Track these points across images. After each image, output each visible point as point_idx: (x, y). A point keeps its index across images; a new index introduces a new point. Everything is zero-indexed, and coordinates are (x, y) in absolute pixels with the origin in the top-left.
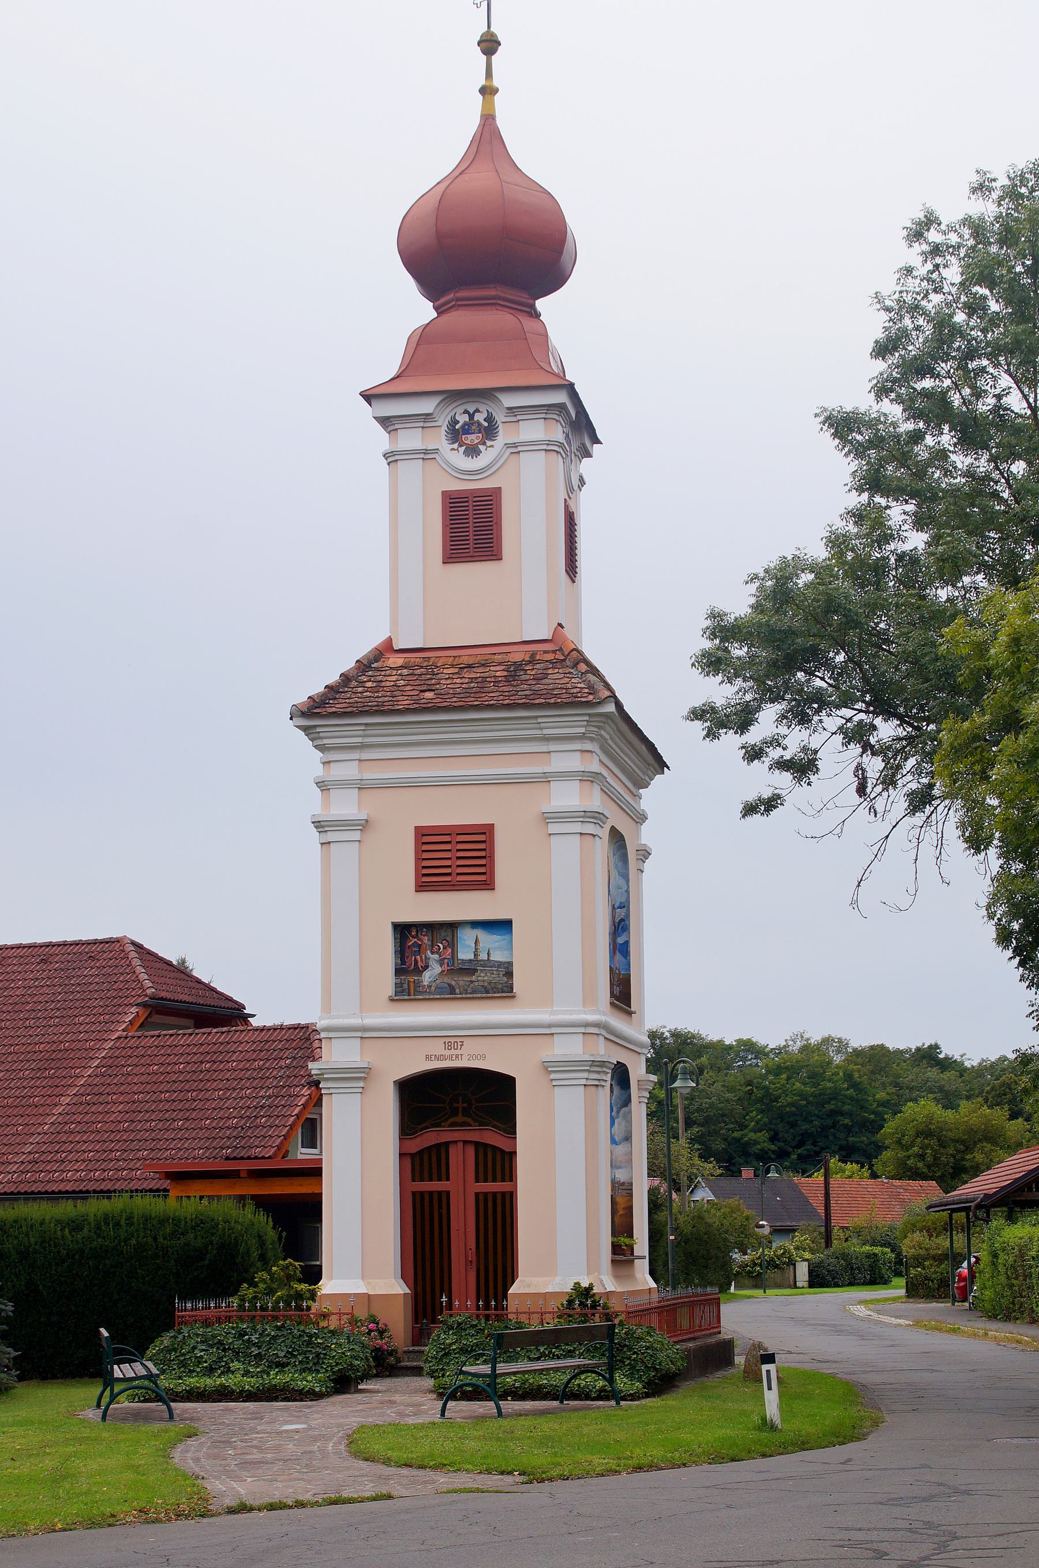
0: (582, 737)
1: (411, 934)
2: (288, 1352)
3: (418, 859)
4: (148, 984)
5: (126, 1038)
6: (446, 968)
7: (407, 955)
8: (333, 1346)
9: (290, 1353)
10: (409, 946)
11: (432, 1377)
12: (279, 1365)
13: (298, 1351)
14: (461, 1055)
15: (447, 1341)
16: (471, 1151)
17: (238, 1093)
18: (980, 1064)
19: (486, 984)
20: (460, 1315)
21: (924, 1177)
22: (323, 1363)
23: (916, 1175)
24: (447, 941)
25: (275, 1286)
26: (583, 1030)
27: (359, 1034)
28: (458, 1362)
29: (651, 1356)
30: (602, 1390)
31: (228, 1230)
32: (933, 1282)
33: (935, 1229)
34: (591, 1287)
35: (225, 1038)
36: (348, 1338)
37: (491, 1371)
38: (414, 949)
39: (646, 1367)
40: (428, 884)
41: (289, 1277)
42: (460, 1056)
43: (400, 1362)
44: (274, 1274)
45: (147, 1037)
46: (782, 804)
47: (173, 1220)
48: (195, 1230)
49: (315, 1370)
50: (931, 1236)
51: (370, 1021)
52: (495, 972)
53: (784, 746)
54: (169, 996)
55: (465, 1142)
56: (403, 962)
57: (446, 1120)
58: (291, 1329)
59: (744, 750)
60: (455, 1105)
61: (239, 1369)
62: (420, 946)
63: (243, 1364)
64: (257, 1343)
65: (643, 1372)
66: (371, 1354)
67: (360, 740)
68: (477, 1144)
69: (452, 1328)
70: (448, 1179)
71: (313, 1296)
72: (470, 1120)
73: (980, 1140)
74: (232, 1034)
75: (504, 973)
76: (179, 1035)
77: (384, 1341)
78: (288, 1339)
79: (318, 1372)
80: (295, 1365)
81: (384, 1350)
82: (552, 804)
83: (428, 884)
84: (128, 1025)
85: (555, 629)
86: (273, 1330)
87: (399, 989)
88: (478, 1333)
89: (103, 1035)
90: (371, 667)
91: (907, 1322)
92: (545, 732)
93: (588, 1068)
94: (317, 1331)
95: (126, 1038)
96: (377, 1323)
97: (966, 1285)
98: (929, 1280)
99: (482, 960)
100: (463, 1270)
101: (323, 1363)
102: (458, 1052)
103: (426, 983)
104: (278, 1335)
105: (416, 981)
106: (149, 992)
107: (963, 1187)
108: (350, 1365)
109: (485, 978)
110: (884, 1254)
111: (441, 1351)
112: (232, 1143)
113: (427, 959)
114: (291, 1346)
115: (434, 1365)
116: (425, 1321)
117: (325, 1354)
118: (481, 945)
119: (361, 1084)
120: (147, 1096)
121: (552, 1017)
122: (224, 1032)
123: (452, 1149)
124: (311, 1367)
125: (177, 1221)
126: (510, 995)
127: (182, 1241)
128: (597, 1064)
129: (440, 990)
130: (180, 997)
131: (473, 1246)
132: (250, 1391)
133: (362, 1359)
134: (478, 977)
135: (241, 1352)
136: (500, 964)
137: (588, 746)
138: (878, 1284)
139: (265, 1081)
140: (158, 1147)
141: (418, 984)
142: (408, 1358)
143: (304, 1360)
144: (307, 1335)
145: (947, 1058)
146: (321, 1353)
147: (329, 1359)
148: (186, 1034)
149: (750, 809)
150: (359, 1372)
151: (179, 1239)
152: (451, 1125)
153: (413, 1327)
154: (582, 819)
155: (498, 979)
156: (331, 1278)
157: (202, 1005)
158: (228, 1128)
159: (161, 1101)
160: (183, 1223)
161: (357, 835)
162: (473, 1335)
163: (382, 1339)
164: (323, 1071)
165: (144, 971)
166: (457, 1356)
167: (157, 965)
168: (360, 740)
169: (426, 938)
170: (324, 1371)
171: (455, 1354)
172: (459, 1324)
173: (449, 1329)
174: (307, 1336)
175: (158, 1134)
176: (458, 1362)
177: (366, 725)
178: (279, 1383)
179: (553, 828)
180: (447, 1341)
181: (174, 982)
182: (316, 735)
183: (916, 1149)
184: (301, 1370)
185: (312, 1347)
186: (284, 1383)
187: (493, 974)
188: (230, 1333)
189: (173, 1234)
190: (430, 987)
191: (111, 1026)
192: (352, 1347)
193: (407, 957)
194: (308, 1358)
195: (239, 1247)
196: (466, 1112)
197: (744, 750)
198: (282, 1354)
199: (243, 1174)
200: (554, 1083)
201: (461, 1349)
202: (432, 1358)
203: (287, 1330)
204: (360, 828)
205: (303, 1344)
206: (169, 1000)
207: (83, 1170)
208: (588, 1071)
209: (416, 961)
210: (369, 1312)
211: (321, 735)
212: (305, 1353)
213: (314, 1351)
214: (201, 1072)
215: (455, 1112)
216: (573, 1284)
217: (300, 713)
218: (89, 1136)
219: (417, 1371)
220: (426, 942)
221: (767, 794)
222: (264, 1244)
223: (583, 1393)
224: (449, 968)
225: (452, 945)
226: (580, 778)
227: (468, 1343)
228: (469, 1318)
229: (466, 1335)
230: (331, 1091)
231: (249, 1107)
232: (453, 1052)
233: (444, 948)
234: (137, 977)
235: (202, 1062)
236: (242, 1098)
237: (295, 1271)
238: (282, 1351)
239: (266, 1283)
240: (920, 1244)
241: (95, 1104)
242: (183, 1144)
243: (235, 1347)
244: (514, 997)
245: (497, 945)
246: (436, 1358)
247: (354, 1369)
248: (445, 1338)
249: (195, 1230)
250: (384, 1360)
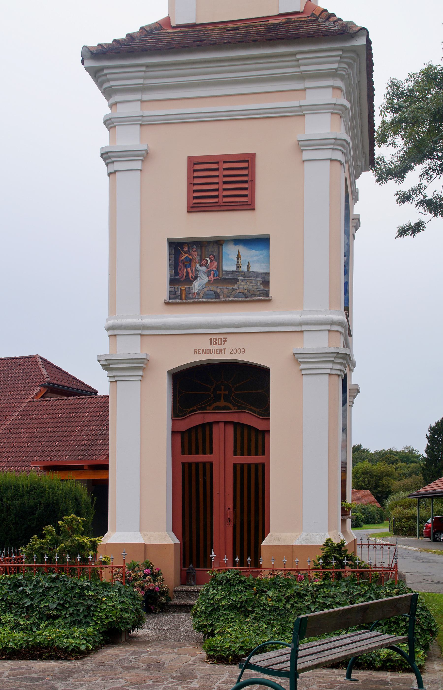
0: (333, 74)
1: (183, 251)
2: (59, 604)
3: (190, 184)
4: (46, 376)
5: (33, 401)
6: (212, 278)
7: (179, 267)
8: (104, 599)
9: (62, 605)
10: (182, 260)
11: (201, 632)
12: (49, 617)
13: (70, 603)
14: (225, 349)
15: (216, 597)
16: (230, 430)
17: (89, 428)
18: (375, 452)
19: (246, 291)
20: (229, 571)
21: (364, 489)
22: (93, 615)
23: (362, 488)
24: (213, 255)
25: (60, 538)
26: (329, 328)
27: (139, 332)
28: (227, 619)
29: (426, 617)
30: (388, 659)
31: (52, 494)
32: (406, 528)
33: (406, 506)
34: (342, 545)
35: (83, 401)
36: (119, 590)
37: (290, 666)
38: (186, 263)
39: (422, 629)
40: (198, 205)
41: (74, 531)
42: (223, 350)
43: (171, 600)
44: (61, 527)
45: (44, 401)
46: (423, 230)
47: (15, 486)
48: (29, 494)
49: (85, 622)
50: (404, 509)
51: (148, 320)
52: (253, 282)
53: (424, 194)
54: (57, 382)
55: (226, 423)
56: (176, 273)
57: (210, 405)
58: (65, 581)
59: (398, 196)
60: (218, 392)
61: (9, 621)
62: (191, 260)
63: (14, 616)
64: (31, 594)
65: (420, 635)
66: (142, 604)
67: (141, 81)
68: (235, 424)
69: (221, 584)
70: (211, 453)
71: (94, 546)
72: (230, 405)
73: (384, 476)
74: (87, 399)
75: (261, 282)
76: (60, 400)
77: (157, 584)
78: (61, 591)
79: (88, 624)
80: (66, 618)
81: (157, 591)
82: (306, 133)
83: (198, 205)
84: (35, 396)
85: (307, 3)
86: (47, 582)
87: (173, 296)
88: (246, 588)
89: (22, 400)
90: (152, 33)
91: (415, 549)
92: (303, 68)
93: (333, 359)
94: (89, 584)
95: (33, 401)
96: (152, 569)
97: (430, 530)
98: (404, 527)
99: (242, 272)
100: (222, 526)
101: (93, 615)
102: (222, 347)
103: (195, 291)
104: (51, 587)
105: (187, 289)
106: (46, 380)
107: (424, 487)
108: (119, 618)
109: (245, 287)
110: (360, 516)
111: (210, 607)
112: (83, 453)
113: (197, 271)
114: (63, 598)
115: (203, 621)
116: (191, 566)
117: (96, 607)
118: (242, 259)
119: (141, 373)
120: (41, 429)
121: (302, 316)
122: (83, 399)
123: (215, 429)
124: (81, 620)
125: (17, 487)
126: (267, 298)
127: (19, 502)
128: (341, 356)
129: (206, 295)
130: (64, 384)
131: (230, 505)
132: (13, 649)
133: (132, 611)
134: (239, 285)
135: (15, 604)
136: (258, 275)
137: (339, 83)
138: (358, 527)
139: (103, 422)
140: (45, 455)
141: (188, 292)
142: (177, 596)
143: (75, 612)
144: (79, 588)
145: (364, 450)
146: (92, 605)
147: (99, 612)
148: (63, 400)
149: (402, 232)
150: (128, 624)
151: (18, 500)
152: (214, 409)
153: (181, 570)
154: (332, 147)
155: (256, 287)
156: (115, 530)
157: (76, 389)
158: (82, 445)
159: (48, 432)
160: (21, 489)
161: (138, 165)
162: (242, 591)
163: (155, 581)
164: (109, 362)
165: (45, 370)
166: (226, 612)
167: (53, 369)
168: (141, 81)
169: (196, 254)
170: (94, 623)
171: (224, 610)
172: (228, 580)
173: (218, 584)
174: (79, 588)
175: (45, 448)
176: (227, 619)
177: (147, 66)
178: (44, 641)
179: (306, 155)
180: (216, 597)
181: (61, 377)
182: (103, 78)
183: (362, 479)
184: (71, 622)
185: (84, 599)
186: (49, 641)
187: (252, 283)
188: (5, 584)
189: (14, 497)
190: (198, 294)
191: (26, 396)
192: (122, 600)
193: (180, 269)
194: (78, 610)
195: (59, 506)
196: (227, 399)
197: (398, 196)
198: (53, 606)
199: (86, 468)
200: (303, 372)
201: (230, 606)
202: (201, 612)
203: (61, 581)
204: (141, 158)
205: (75, 597)
206: (58, 385)
207: (4, 467)
208: (333, 362)
209: (187, 273)
210: (145, 558)
211: (109, 76)
212: (76, 605)
213: (85, 603)
214: (70, 417)
215: (218, 399)
216: (325, 541)
217: (90, 53)
218: (9, 450)
219: (186, 608)
220: (196, 257)
221: (414, 222)
222: (80, 504)
223: (366, 662)
224: (215, 278)
225: (218, 259)
226: (331, 111)
227: (237, 600)
228: (238, 574)
229: (235, 591)
230: (116, 379)
231: (93, 435)
232: (217, 347)
233: (211, 262)
234: (42, 373)
235: (70, 413)
236: (90, 430)
237: (78, 525)
238: (54, 603)
239: (52, 535)
240: (400, 512)
241: (14, 433)
242: (58, 454)
243: (8, 598)
244: (270, 300)
245: (255, 258)
246: (205, 613)
247: (124, 622)
248: (214, 593)
249: (29, 494)
250: (157, 599)
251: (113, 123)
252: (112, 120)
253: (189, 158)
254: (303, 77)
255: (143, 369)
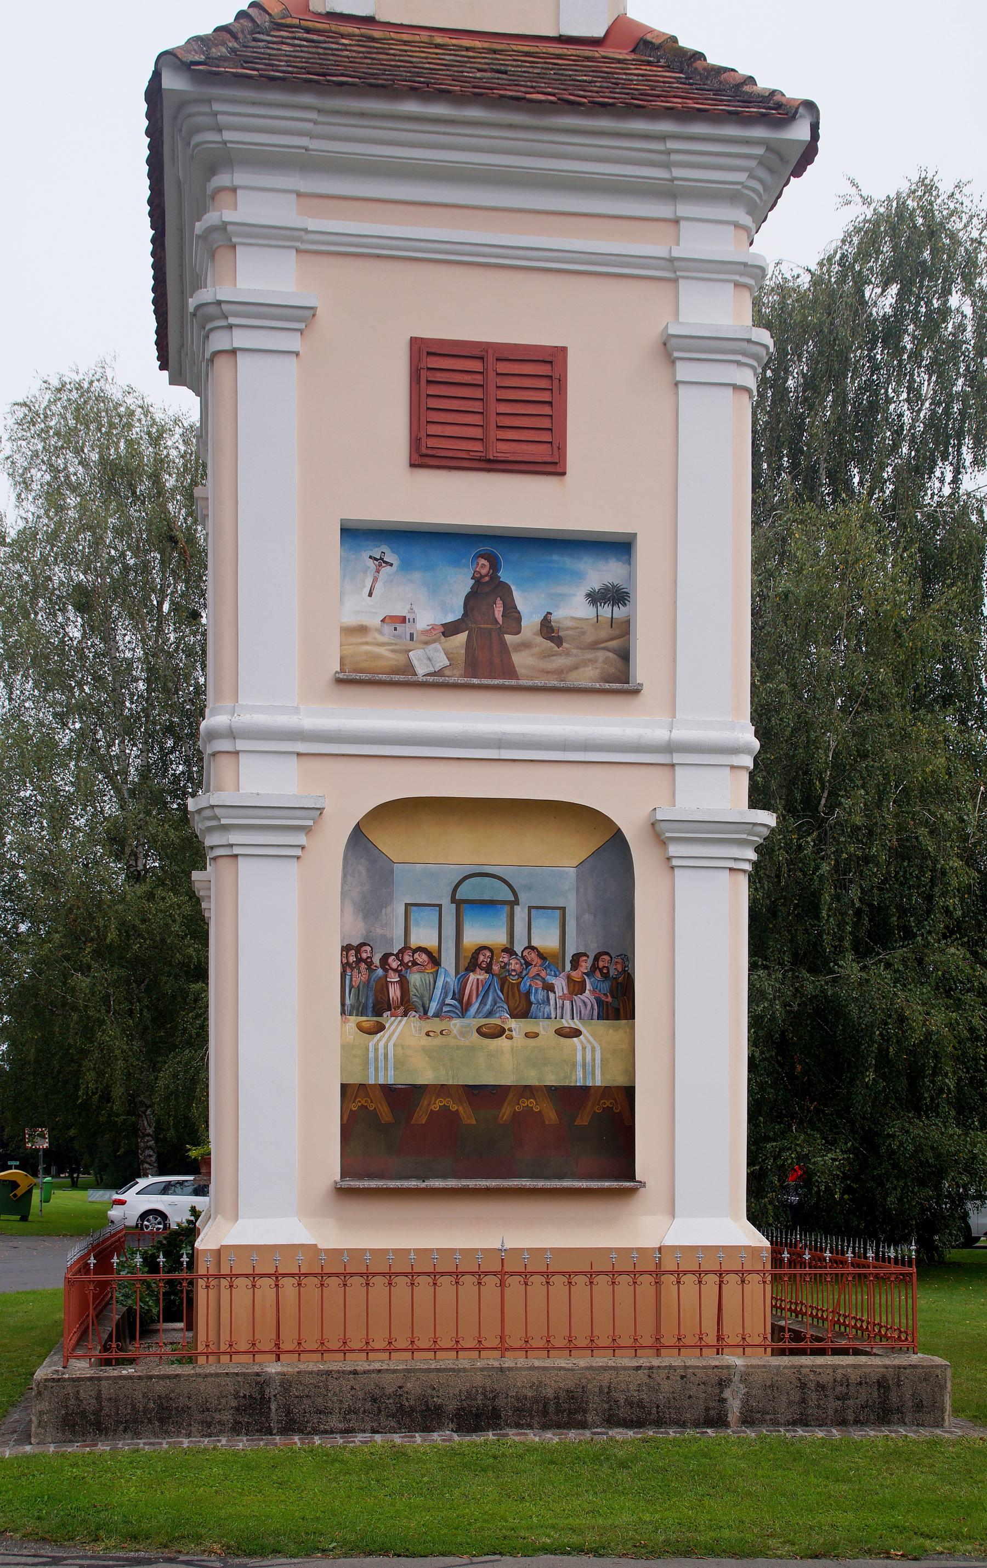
154: (739, 358)
179: (684, 371)
244: (636, 692)
251: (227, 318)
252: (217, 811)
253: (413, 341)
254: (671, 193)
255: (307, 830)
